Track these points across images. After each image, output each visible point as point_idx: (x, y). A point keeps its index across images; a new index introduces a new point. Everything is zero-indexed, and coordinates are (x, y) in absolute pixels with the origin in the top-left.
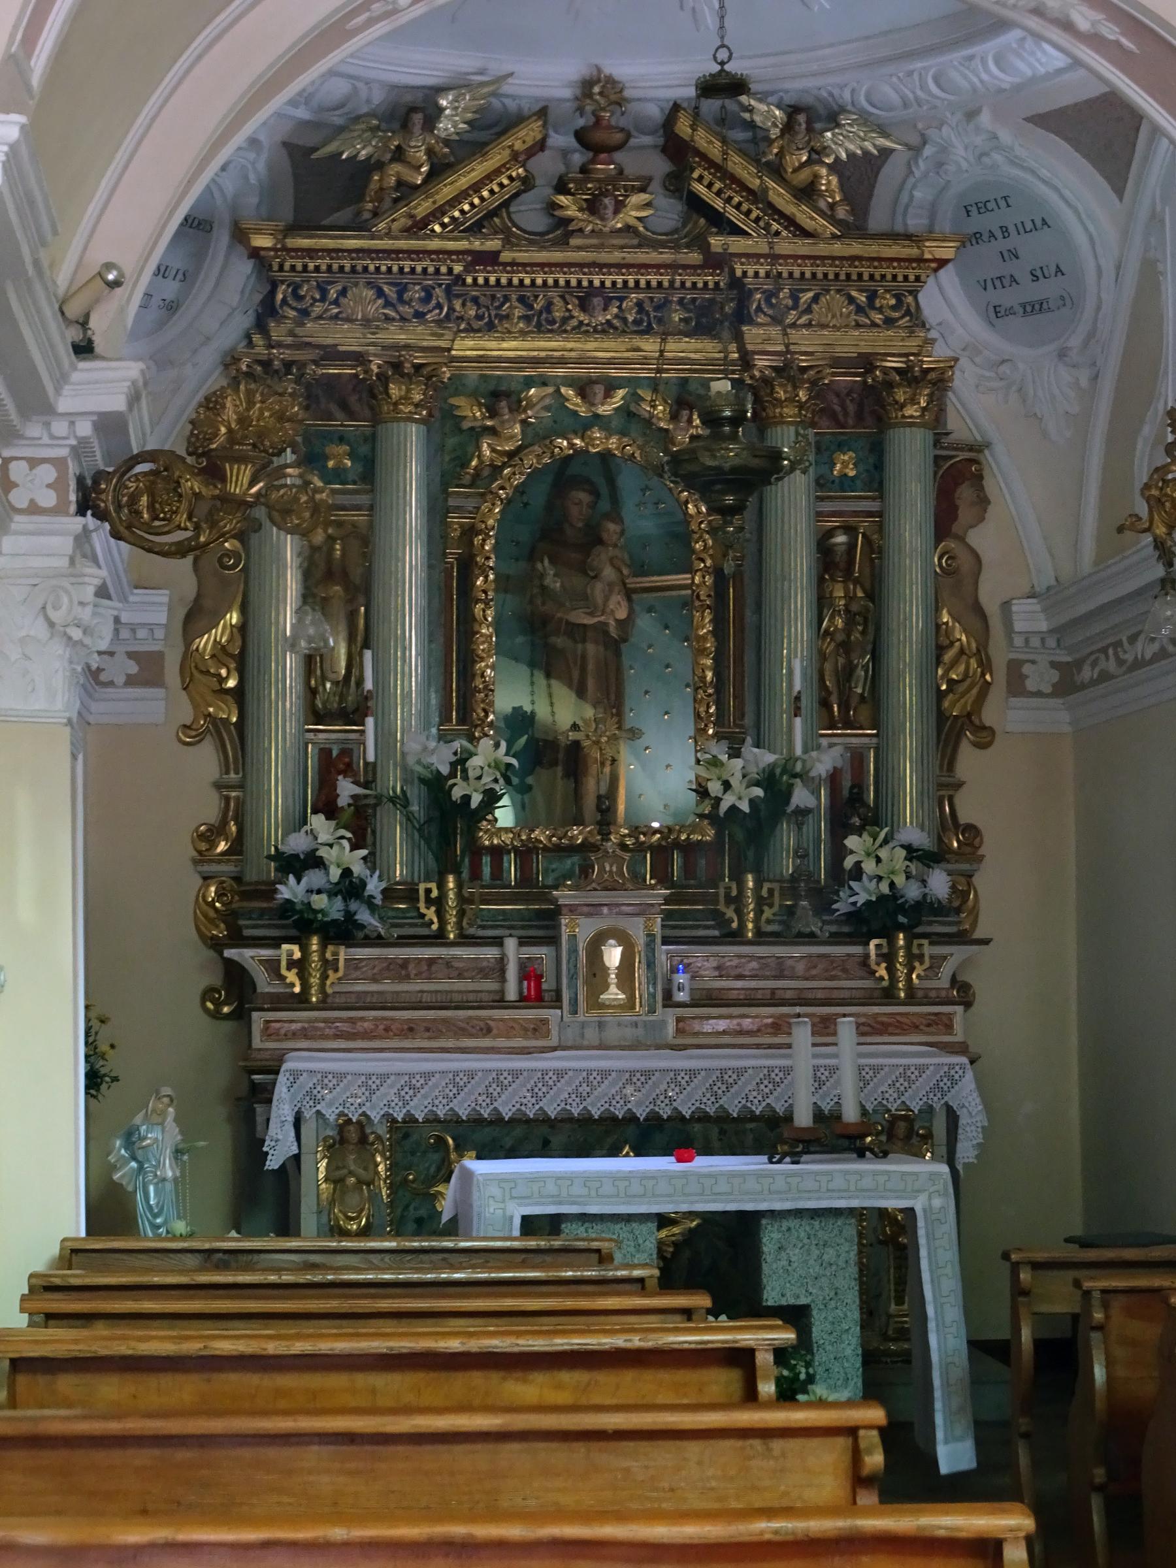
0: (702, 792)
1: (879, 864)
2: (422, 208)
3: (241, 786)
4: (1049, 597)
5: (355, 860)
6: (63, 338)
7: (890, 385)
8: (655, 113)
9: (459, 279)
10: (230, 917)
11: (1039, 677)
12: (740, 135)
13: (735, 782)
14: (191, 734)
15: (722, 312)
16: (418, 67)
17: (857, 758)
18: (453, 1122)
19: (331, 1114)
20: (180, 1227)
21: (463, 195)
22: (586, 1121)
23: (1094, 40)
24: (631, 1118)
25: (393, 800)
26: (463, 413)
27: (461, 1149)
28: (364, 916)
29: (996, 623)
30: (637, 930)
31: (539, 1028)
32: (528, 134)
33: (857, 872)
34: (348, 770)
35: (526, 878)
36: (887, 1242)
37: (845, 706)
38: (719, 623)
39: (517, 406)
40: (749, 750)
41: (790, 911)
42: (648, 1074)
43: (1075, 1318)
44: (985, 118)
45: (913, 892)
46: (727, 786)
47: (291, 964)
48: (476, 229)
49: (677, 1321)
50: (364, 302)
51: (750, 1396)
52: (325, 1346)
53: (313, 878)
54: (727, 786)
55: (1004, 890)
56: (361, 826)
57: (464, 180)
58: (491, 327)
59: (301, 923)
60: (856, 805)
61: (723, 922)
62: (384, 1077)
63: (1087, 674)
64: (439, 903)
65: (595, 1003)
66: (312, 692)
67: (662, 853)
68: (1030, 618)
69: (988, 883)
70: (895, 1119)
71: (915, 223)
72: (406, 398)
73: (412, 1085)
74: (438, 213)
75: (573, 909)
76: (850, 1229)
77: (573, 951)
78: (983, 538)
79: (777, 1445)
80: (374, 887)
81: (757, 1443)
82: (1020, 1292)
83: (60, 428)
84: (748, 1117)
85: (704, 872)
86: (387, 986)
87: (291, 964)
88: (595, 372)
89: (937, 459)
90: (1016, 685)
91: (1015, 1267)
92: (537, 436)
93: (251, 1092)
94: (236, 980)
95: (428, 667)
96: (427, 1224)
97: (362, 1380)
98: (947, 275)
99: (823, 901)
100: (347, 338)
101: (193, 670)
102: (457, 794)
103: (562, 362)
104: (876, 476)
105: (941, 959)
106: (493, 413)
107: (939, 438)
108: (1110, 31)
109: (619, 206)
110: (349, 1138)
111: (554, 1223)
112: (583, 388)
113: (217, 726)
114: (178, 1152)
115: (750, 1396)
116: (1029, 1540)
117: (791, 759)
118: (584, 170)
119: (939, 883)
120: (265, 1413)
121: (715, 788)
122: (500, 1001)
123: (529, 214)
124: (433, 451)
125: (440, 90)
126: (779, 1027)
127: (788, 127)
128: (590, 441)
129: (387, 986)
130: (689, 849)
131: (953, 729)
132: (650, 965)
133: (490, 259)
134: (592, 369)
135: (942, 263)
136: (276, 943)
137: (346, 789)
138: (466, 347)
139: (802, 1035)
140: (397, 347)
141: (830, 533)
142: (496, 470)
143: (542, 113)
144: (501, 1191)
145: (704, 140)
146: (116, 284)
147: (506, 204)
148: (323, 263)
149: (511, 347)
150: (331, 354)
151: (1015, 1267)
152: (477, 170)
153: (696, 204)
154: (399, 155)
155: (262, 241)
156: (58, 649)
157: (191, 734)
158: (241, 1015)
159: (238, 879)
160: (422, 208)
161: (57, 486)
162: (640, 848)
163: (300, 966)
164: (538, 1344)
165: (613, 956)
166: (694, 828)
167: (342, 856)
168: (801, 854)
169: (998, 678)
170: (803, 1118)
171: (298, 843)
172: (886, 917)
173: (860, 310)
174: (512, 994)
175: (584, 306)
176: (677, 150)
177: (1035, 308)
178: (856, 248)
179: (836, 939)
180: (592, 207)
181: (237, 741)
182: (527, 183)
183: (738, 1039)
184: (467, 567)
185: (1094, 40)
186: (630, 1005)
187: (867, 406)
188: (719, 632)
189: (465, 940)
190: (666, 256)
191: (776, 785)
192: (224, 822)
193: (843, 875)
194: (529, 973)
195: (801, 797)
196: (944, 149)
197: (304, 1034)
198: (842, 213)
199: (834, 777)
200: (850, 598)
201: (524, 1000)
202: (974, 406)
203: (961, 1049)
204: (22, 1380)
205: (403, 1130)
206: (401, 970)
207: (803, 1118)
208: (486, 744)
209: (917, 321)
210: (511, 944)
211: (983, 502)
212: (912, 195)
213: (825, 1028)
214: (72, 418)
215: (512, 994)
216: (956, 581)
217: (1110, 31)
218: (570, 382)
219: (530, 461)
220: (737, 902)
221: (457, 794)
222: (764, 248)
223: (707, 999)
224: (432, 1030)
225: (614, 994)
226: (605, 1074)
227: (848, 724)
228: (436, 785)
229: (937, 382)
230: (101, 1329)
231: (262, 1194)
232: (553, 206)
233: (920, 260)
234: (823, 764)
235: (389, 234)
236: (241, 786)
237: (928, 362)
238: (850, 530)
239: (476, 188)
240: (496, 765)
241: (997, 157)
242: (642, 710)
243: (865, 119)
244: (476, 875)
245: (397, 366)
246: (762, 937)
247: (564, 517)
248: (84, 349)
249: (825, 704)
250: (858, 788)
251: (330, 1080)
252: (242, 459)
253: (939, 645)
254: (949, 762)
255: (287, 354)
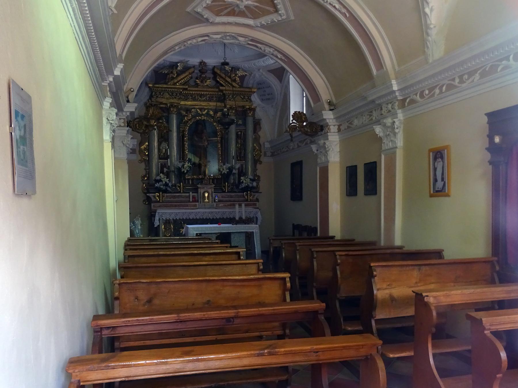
0: (219, 170)
1: (245, 181)
2: (176, 81)
3: (149, 169)
4: (270, 142)
5: (167, 180)
6: (125, 99)
7: (247, 110)
8: (211, 67)
9: (181, 92)
10: (147, 189)
11: (269, 154)
12: (224, 71)
13: (225, 169)
14: (141, 161)
15: (222, 99)
16: (175, 59)
17: (242, 165)
18: (183, 220)
19: (164, 219)
20: (142, 236)
21: (182, 79)
22: (203, 219)
23: (281, 59)
24: (210, 219)
25: (173, 171)
26: (182, 113)
27: (184, 224)
28: (169, 189)
29: (262, 147)
30: (210, 191)
31: (195, 206)
32: (191, 70)
33: (243, 182)
34: (166, 167)
35: (193, 183)
36: (249, 236)
37: (240, 158)
38: (221, 145)
39: (190, 112)
40: (226, 164)
41: (232, 188)
42: (212, 212)
43: (280, 247)
44: (261, 70)
45: (251, 185)
46: (223, 169)
47: (157, 196)
48: (184, 85)
49: (225, 248)
50: (167, 95)
51: (239, 259)
52: (149, 253)
53: (161, 183)
54: (223, 169)
55: (264, 185)
56: (168, 175)
57: (182, 77)
58: (186, 100)
59: (159, 190)
60: (242, 173)
61: (222, 190)
62: (172, 213)
63: (276, 153)
64: (180, 187)
65: (204, 202)
66: (159, 155)
67: (213, 179)
68: (267, 145)
69: (261, 184)
70: (249, 218)
71: (250, 86)
72: (173, 111)
73: (177, 214)
74: (178, 82)
75: (200, 188)
76: (244, 235)
77: (200, 194)
78: (260, 133)
79: (247, 265)
80: (170, 184)
81: (244, 265)
82: (270, 243)
83: (124, 114)
84: (227, 218)
85: (220, 182)
86: (172, 199)
87: (157, 196)
88: (202, 107)
89: (254, 122)
90: (265, 155)
91: (270, 240)
92: (193, 117)
93: (151, 216)
94: (148, 198)
95: (177, 152)
96: (180, 235)
97: (182, 257)
98: (255, 94)
99: (237, 186)
100: (164, 101)
101: (141, 152)
102: (183, 170)
103: (197, 105)
104: (245, 124)
105: (254, 195)
106: (187, 113)
107: (254, 118)
108: (283, 58)
109: (206, 82)
110: (167, 222)
111: (201, 234)
112: (201, 109)
113: (145, 160)
114: (141, 225)
115: (239, 259)
116: (290, 278)
117: (233, 165)
118: (200, 76)
119: (255, 184)
120: (180, 262)
121: (221, 170)
122: (189, 202)
123: (192, 83)
124: (177, 119)
125: (178, 63)
126: (234, 205)
127: (231, 71)
128: (202, 118)
129: (172, 199)
130: (217, 179)
131: (256, 161)
132: (212, 196)
133: (186, 89)
134: (204, 106)
135: (255, 92)
136: (155, 193)
137: (165, 170)
138: (182, 103)
139: (237, 206)
140: (172, 102)
141: (238, 132)
142: (187, 122)
143: (194, 67)
144: (193, 229)
145: (218, 72)
146: (133, 91)
147: (188, 81)
148: (160, 89)
149: (189, 103)
150: (161, 103)
151: (270, 240)
152: (184, 75)
153: (217, 82)
154: (172, 72)
155: (151, 85)
156: (125, 148)
157: (141, 161)
158: (150, 204)
159: (148, 183)
160: (176, 81)
161: (124, 123)
162: (210, 179)
163: (159, 196)
164: (208, 252)
165: (206, 195)
166: (218, 176)
167: (165, 180)
168: (234, 179)
169: (262, 154)
170: (237, 218)
171: (158, 178)
172: (247, 189)
173: (242, 99)
174: (191, 200)
175: (201, 97)
176: (214, 73)
177: (269, 99)
178: (242, 89)
179: (239, 192)
180: (202, 82)
181: (148, 163)
182: (191, 78)
183: (225, 207)
184: (183, 136)
185: (281, 59)
186: (209, 202)
187: (244, 113)
188: (221, 147)
189: (184, 192)
190: (212, 90)
191: (231, 169)
192: (146, 174)
193: (240, 183)
194: (194, 197)
195: (234, 171)
196: (255, 75)
197: (160, 207)
198: (240, 84)
199: (239, 169)
200: (241, 142)
201: (193, 201)
202: (259, 113)
203: (258, 208)
204: (130, 258)
205: (175, 221)
206: (174, 197)
207: (237, 218)
208: (187, 163)
209: (251, 101)
210: (191, 193)
211: (260, 128)
212: (250, 82)
213: (240, 205)
214: (126, 112)
215: (191, 200)
216: (257, 140)
217: (283, 58)
218: (199, 108)
219: (193, 121)
220: (225, 187)
221: (183, 170)
222: (231, 89)
223: (220, 201)
224: (179, 206)
225: (207, 200)
226: (206, 212)
227: (241, 160)
228: (179, 169)
229: (254, 110)
230: (138, 251)
231: (152, 230)
232: (195, 81)
233: (251, 92)
234: (237, 166)
235: (170, 85)
236: (149, 169)
237: (253, 107)
238: (241, 132)
239: (184, 78)
240: (189, 166)
241: (263, 76)
242: (209, 158)
243: (243, 70)
244: (185, 183)
245: (172, 105)
246: (228, 192)
247: (198, 129)
248: (128, 101)
249: (237, 158)
250: (242, 170)
251: (164, 214)
252: (153, 119)
253: (254, 149)
254: (255, 166)
255: (155, 103)
